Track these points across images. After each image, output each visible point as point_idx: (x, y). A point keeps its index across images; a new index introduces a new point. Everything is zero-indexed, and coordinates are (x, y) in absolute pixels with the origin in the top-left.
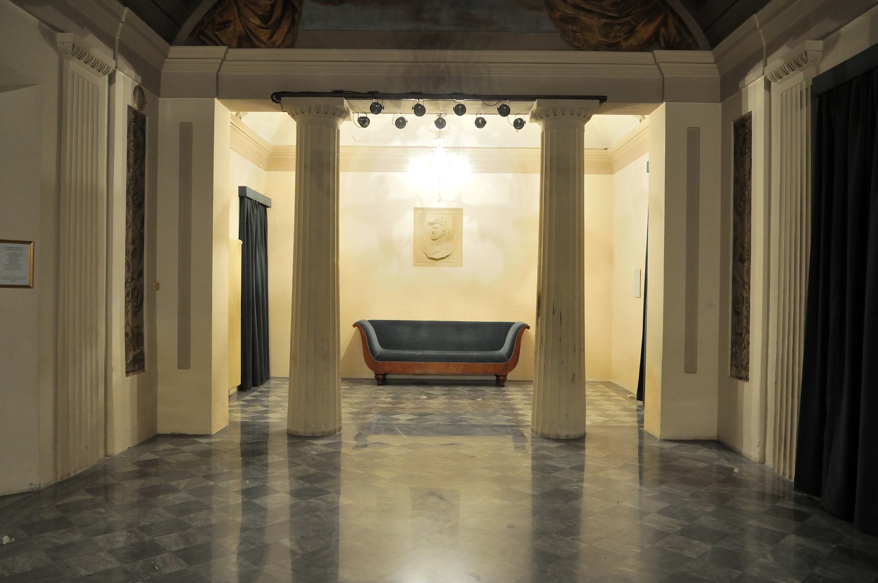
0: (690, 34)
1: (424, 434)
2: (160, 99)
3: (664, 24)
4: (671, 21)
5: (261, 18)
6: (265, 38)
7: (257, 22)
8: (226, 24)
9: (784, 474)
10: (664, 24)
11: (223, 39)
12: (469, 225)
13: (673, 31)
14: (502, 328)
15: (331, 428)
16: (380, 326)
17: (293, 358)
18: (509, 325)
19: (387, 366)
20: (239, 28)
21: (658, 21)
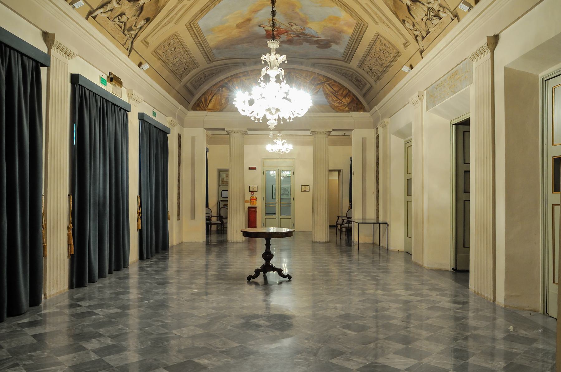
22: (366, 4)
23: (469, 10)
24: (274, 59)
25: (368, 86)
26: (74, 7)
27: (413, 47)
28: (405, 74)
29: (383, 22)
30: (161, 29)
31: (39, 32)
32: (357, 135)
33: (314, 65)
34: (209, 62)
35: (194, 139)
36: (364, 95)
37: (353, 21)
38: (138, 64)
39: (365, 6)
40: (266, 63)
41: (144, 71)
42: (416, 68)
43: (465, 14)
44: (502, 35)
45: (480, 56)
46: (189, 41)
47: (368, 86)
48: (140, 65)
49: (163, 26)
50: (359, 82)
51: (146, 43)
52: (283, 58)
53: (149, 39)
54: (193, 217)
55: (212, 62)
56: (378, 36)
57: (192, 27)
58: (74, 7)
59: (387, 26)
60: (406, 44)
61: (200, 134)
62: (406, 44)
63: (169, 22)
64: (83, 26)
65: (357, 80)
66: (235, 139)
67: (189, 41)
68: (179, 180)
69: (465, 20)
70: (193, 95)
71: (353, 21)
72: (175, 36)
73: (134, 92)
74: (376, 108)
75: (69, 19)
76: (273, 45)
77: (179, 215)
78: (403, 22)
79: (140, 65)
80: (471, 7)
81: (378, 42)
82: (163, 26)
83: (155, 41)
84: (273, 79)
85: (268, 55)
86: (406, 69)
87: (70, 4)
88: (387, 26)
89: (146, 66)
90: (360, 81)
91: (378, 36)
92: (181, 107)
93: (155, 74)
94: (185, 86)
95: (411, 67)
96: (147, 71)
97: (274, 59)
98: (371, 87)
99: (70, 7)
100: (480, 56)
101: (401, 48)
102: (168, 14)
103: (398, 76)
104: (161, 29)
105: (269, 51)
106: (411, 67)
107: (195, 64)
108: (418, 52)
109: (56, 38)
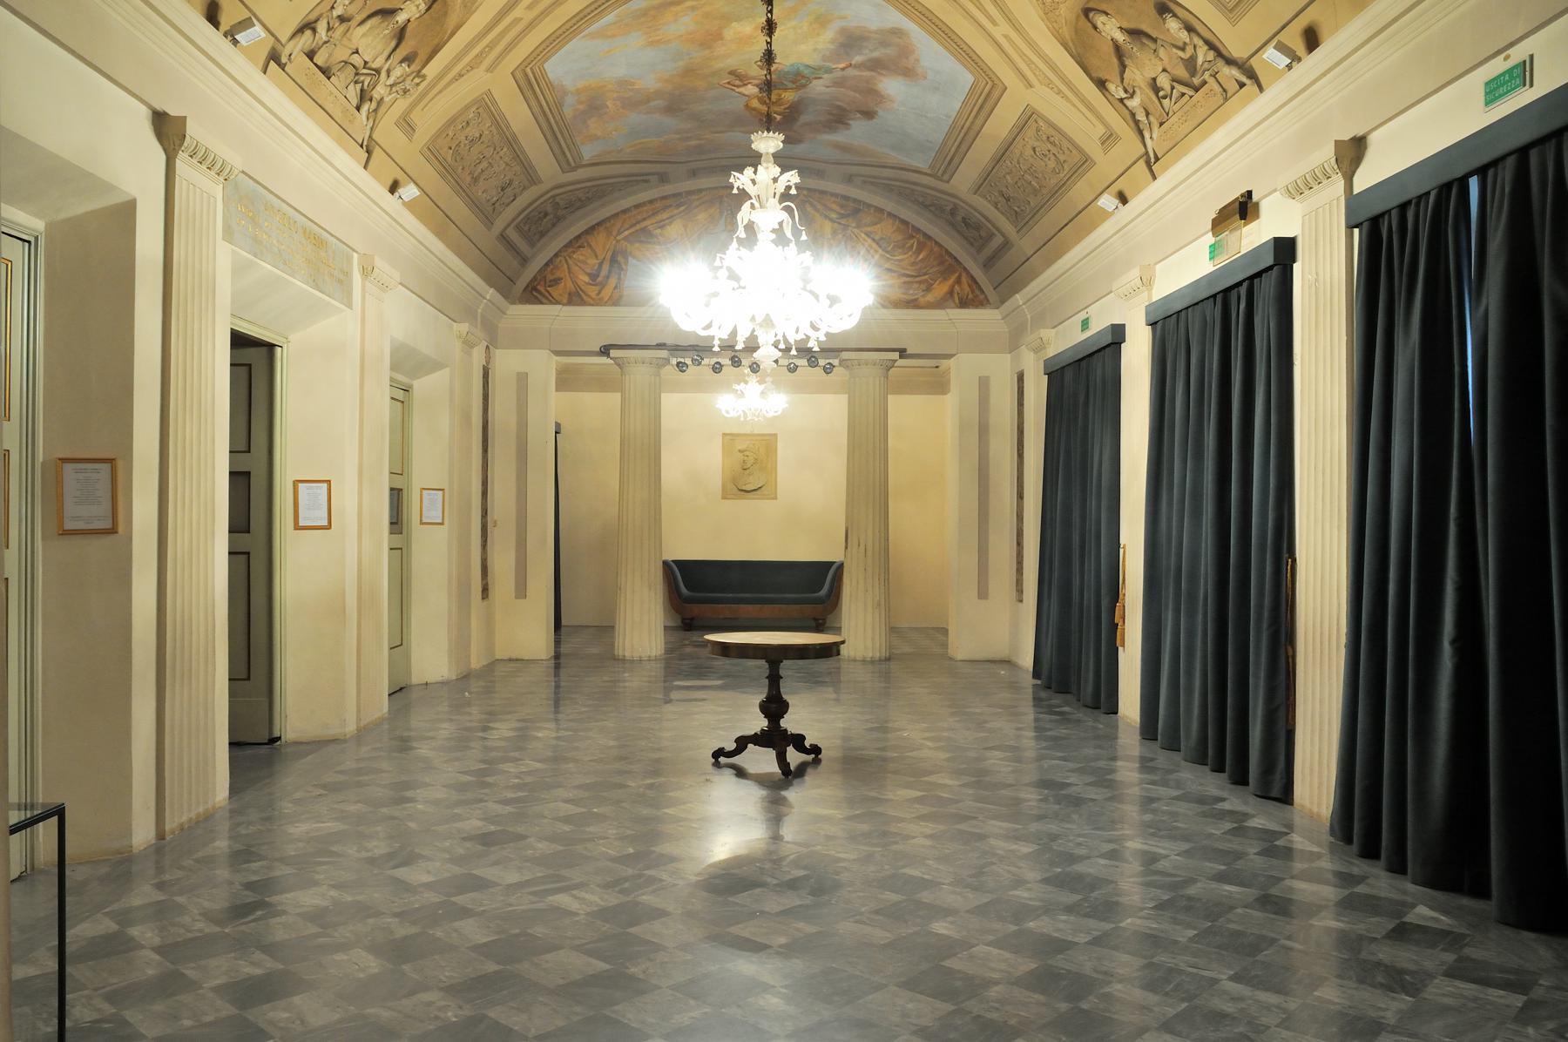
0: (982, 291)
1: (1267, 990)
2: (497, 351)
3: (958, 281)
4: (964, 279)
5: (589, 275)
6: (593, 295)
7: (586, 279)
8: (556, 281)
9: (1319, 805)
10: (958, 281)
11: (555, 294)
12: (783, 452)
13: (966, 286)
14: (828, 565)
15: (1076, 157)
16: (684, 565)
17: (117, 205)
18: (832, 563)
19: (696, 609)
20: (570, 284)
21: (951, 281)
22: (1006, 36)
23: (1289, 67)
24: (765, 183)
25: (997, 241)
26: (235, 42)
27: (1129, 145)
28: (1105, 215)
29: (1049, 84)
30: (445, 87)
31: (144, 113)
32: (963, 368)
33: (849, 179)
34: (565, 166)
35: (522, 379)
36: (988, 264)
37: (966, 79)
38: (390, 182)
39: (1002, 41)
40: (744, 195)
41: (404, 204)
42: (1135, 204)
43: (1279, 74)
44: (1373, 139)
45: (1316, 187)
46: (519, 115)
47: (997, 241)
48: (394, 188)
49: (455, 79)
50: (972, 229)
51: (407, 125)
52: (793, 177)
53: (415, 117)
54: (521, 591)
55: (574, 169)
56: (1029, 117)
57: (530, 82)
58: (235, 42)
59: (1059, 92)
60: (1109, 139)
61: (541, 365)
62: (1109, 139)
63: (471, 67)
64: (249, 86)
65: (967, 225)
66: (639, 374)
67: (519, 115)
68: (484, 493)
69: (1276, 92)
70: (524, 261)
71: (966, 79)
72: (485, 105)
73: (379, 263)
74: (1019, 298)
75: (203, 58)
76: (768, 143)
77: (485, 590)
78: (1101, 84)
79: (394, 188)
80: (1295, 59)
81: (1030, 132)
82: (455, 79)
83: (430, 119)
84: (765, 236)
85: (749, 171)
86: (1108, 202)
87: (225, 35)
88: (1059, 92)
89: (409, 192)
90: (978, 227)
91: (1029, 117)
92: (491, 293)
93: (432, 212)
94: (503, 237)
95: (1123, 199)
96: (410, 205)
97: (765, 183)
98: (1006, 245)
99: (226, 44)
100: (1316, 187)
101: (1093, 149)
102: (470, 46)
103: (1082, 220)
104: (445, 87)
105: (754, 160)
106: (1123, 199)
107: (530, 176)
108: (1142, 163)
109: (192, 129)
